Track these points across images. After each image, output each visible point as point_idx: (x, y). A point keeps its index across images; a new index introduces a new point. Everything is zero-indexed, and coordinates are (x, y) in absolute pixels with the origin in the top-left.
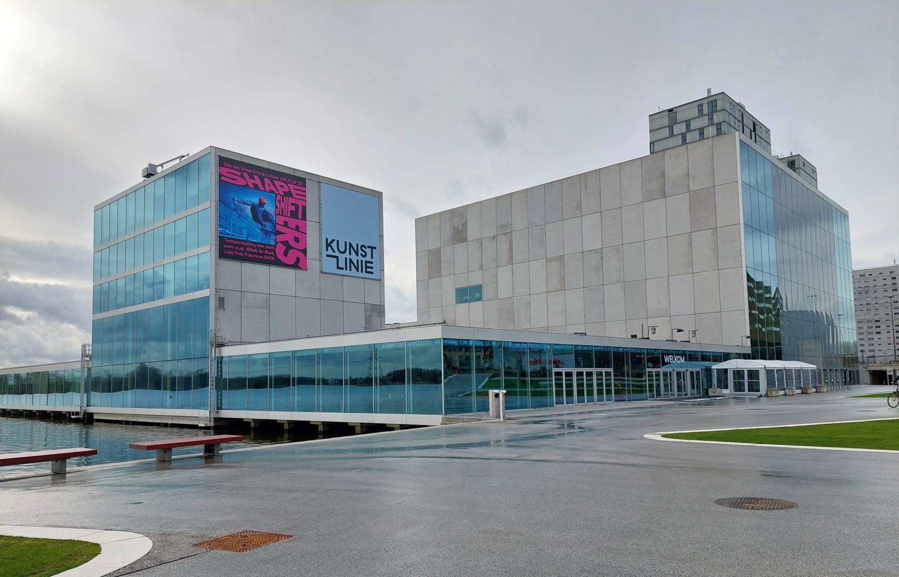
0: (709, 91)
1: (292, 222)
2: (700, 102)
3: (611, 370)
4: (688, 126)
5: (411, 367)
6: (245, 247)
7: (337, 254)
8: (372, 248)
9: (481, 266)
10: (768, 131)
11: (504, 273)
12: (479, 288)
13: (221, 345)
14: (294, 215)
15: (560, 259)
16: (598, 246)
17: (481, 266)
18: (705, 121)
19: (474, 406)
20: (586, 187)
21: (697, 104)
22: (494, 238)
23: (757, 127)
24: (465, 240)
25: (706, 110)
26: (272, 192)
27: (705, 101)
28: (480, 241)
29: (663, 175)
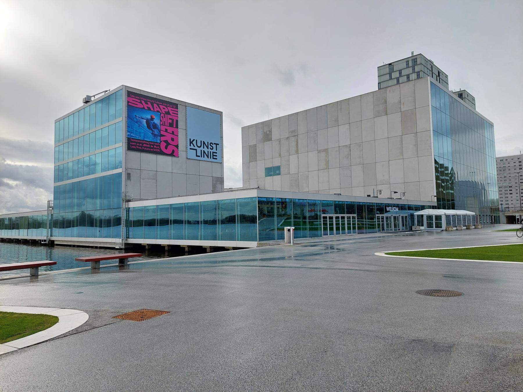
0: (412, 53)
1: (170, 129)
2: (407, 60)
3: (355, 215)
4: (400, 73)
5: (239, 214)
7: (196, 148)
8: (217, 144)
9: (280, 155)
10: (447, 76)
11: (293, 159)
12: (278, 168)
13: (129, 201)
14: (171, 125)
15: (326, 151)
16: (348, 143)
17: (280, 155)
18: (410, 70)
20: (341, 109)
21: (405, 60)
22: (287, 138)
23: (440, 74)
24: (270, 140)
25: (410, 64)
27: (410, 59)
28: (279, 141)
29: (386, 102)
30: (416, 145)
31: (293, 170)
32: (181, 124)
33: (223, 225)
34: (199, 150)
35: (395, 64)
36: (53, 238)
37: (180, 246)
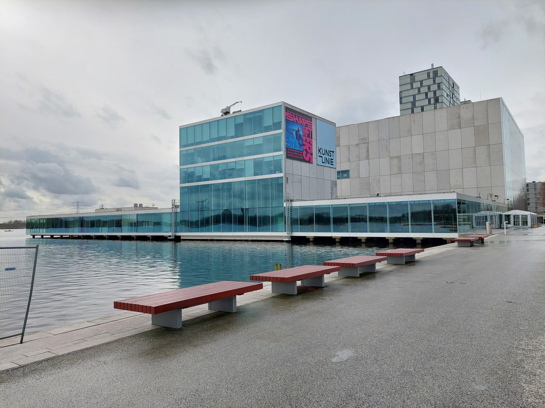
0: (432, 65)
1: (308, 139)
4: (421, 84)
5: (213, 215)
6: (294, 152)
7: (322, 155)
8: (333, 152)
9: (349, 160)
11: (363, 164)
12: (347, 172)
13: (291, 201)
14: (308, 136)
15: (399, 158)
16: (421, 151)
17: (349, 160)
19: (368, 229)
20: (414, 121)
21: (427, 72)
22: (357, 145)
25: (431, 76)
26: (301, 124)
27: (432, 71)
28: (348, 147)
30: (489, 156)
31: (363, 174)
32: (314, 137)
33: (302, 226)
34: (323, 156)
35: (416, 74)
36: (178, 234)
37: (385, 238)
